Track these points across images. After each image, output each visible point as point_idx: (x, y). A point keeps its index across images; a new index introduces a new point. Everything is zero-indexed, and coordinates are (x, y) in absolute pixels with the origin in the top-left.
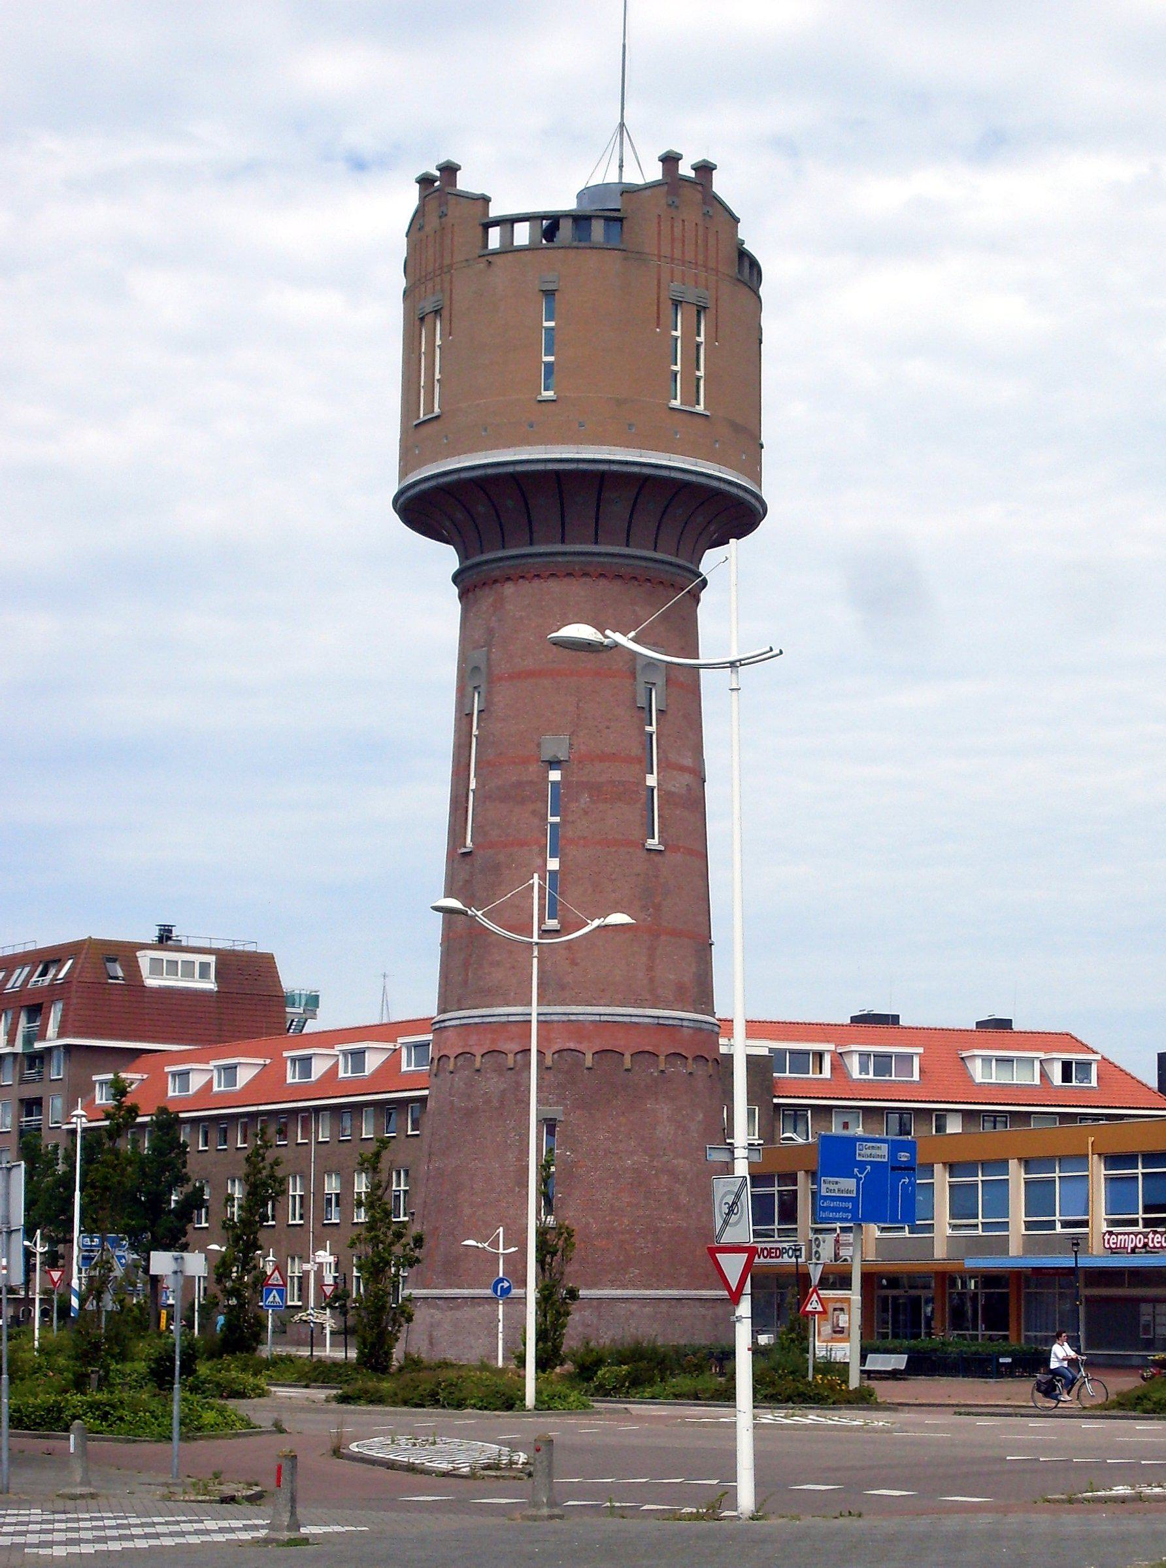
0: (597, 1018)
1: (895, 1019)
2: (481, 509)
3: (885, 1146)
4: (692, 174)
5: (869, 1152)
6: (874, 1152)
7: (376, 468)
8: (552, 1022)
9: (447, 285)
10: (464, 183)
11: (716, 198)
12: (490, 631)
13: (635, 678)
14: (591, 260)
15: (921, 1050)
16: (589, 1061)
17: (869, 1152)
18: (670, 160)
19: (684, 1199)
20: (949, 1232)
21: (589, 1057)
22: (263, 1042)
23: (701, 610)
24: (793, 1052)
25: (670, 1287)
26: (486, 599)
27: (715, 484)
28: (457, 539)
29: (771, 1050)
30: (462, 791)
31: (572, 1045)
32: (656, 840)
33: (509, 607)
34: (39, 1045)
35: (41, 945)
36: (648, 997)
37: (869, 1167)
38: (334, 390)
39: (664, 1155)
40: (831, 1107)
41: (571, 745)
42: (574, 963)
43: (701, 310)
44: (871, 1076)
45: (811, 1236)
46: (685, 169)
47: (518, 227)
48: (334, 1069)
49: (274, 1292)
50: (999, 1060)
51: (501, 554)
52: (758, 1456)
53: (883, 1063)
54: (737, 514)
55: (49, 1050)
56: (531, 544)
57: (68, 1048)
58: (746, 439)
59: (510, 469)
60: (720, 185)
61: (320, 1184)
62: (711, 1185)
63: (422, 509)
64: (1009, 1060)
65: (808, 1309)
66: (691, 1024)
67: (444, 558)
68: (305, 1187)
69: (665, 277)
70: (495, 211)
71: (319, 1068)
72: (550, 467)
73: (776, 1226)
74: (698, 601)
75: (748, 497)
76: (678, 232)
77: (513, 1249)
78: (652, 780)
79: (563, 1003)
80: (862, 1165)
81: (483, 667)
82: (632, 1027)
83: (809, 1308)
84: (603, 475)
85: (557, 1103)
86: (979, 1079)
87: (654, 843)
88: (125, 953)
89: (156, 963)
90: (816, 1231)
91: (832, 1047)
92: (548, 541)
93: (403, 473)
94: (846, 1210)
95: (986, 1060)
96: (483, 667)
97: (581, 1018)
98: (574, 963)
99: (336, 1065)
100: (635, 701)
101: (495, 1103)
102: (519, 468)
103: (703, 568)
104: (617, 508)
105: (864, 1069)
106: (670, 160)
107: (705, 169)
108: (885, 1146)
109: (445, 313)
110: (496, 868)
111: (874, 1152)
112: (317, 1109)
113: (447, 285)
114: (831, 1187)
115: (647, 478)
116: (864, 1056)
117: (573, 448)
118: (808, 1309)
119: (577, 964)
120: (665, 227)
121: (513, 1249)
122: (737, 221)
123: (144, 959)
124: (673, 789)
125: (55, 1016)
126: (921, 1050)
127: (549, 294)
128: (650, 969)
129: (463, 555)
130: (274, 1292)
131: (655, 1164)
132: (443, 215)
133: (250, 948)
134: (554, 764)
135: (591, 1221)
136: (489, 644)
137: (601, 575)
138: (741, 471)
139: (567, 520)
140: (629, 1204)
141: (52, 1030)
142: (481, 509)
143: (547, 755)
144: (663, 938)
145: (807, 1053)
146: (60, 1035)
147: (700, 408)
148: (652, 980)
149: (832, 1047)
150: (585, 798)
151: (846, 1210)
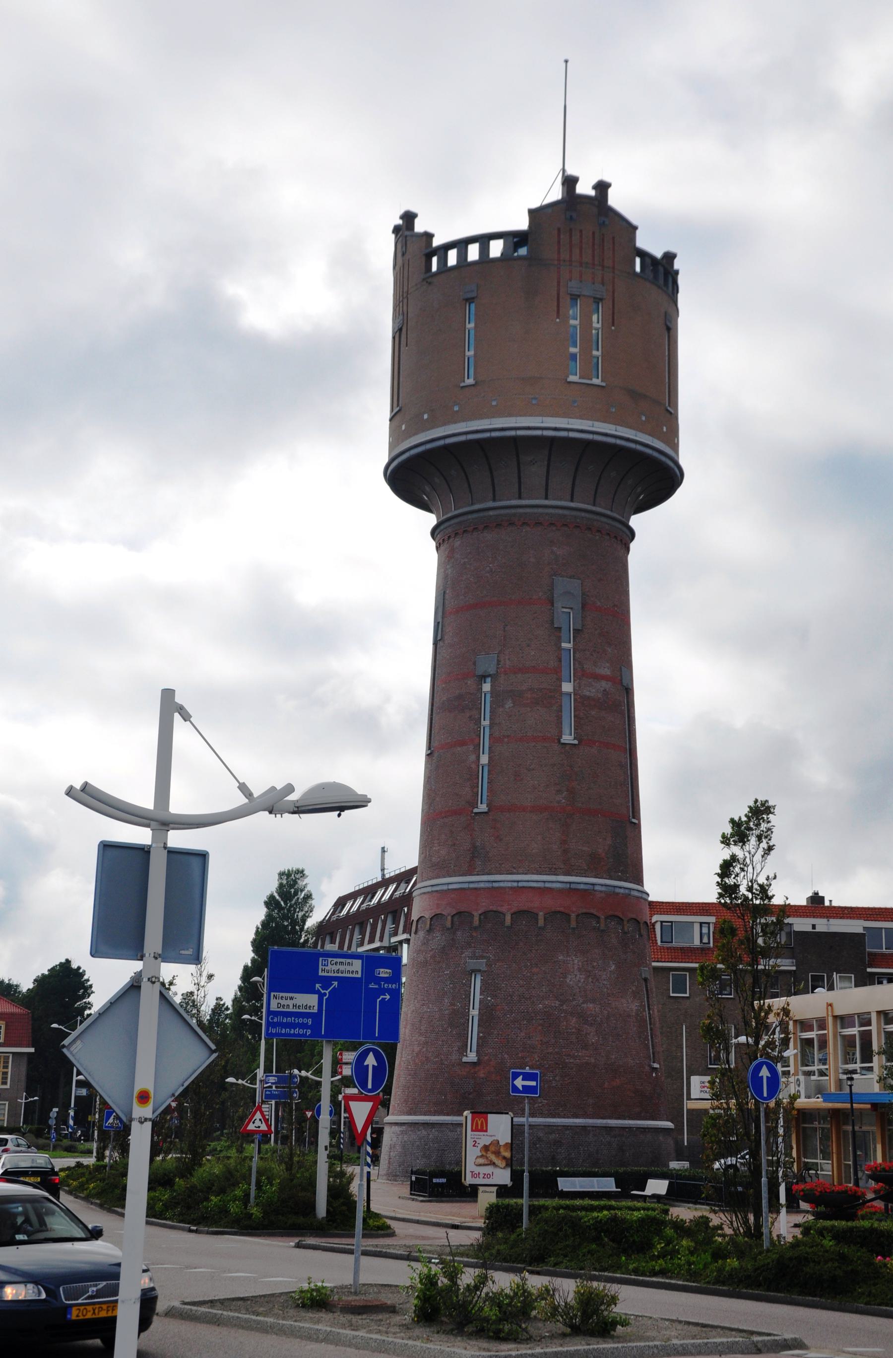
0: (515, 884)
5: (335, 968)
6: (342, 968)
8: (480, 889)
10: (420, 227)
11: (611, 210)
13: (552, 605)
17: (335, 968)
18: (570, 182)
19: (593, 1039)
23: (631, 558)
25: (576, 1116)
36: (562, 866)
37: (336, 983)
39: (574, 999)
41: (499, 661)
56: (472, 504)
60: (614, 200)
65: (249, 1128)
66: (603, 889)
70: (436, 242)
80: (326, 981)
82: (543, 891)
83: (251, 1127)
87: (568, 738)
94: (304, 1026)
97: (502, 884)
100: (552, 623)
104: (535, 472)
106: (570, 182)
107: (602, 187)
111: (342, 968)
114: (283, 1002)
115: (553, 439)
118: (249, 1128)
119: (501, 840)
122: (635, 228)
124: (588, 693)
128: (564, 842)
131: (565, 1007)
135: (506, 1056)
139: (496, 481)
143: (480, 672)
148: (565, 851)
150: (509, 704)
151: (304, 1026)
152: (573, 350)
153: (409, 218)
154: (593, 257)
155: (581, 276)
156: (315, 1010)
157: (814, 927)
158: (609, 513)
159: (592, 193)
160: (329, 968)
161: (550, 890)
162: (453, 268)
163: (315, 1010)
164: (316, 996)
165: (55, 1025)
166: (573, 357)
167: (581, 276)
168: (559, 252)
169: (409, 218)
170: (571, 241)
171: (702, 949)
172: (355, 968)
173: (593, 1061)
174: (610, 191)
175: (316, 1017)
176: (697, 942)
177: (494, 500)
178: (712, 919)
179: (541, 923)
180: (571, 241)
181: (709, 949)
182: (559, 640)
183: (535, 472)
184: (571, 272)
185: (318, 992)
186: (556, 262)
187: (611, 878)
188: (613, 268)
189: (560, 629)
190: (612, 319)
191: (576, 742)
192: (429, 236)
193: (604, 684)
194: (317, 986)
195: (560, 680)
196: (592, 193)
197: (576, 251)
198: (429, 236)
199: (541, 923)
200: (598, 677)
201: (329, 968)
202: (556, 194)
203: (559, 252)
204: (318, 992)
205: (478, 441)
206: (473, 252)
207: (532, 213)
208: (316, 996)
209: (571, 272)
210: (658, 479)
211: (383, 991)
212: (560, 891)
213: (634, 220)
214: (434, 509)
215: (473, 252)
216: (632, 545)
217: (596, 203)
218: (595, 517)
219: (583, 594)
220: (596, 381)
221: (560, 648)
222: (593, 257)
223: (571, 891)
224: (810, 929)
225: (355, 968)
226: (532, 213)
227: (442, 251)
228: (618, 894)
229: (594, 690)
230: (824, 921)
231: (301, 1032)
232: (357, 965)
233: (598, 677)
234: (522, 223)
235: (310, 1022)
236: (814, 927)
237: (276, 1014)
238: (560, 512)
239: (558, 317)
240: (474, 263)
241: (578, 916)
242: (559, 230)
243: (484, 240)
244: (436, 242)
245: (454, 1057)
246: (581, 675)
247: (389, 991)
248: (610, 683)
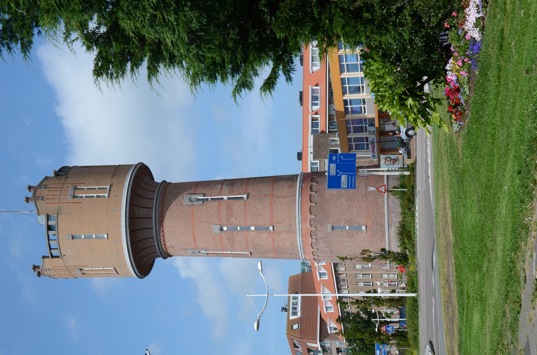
1: (301, 93)
2: (143, 253)
3: (331, 165)
4: (32, 192)
9: (72, 268)
12: (181, 249)
14: (61, 226)
15: (310, 86)
16: (313, 216)
20: (365, 94)
21: (312, 216)
22: (316, 285)
23: (173, 181)
24: (312, 127)
26: (170, 251)
27: (131, 182)
28: (153, 259)
29: (312, 134)
30: (232, 255)
31: (309, 222)
32: (244, 196)
33: (173, 244)
34: (320, 349)
35: (289, 348)
40: (329, 114)
42: (283, 222)
43: (76, 189)
44: (319, 102)
45: (367, 133)
46: (30, 195)
48: (323, 266)
50: (313, 61)
51: (157, 247)
52: (405, 297)
53: (315, 98)
55: (321, 346)
56: (153, 238)
57: (320, 341)
59: (130, 247)
61: (359, 270)
64: (313, 57)
68: (359, 274)
69: (65, 201)
71: (323, 271)
72: (128, 235)
73: (365, 143)
75: (136, 169)
76: (51, 197)
78: (225, 198)
79: (296, 225)
81: (193, 251)
84: (130, 218)
85: (327, 226)
86: (319, 68)
88: (291, 324)
89: (295, 314)
90: (366, 131)
91: (310, 115)
92: (152, 233)
94: (352, 179)
95: (313, 65)
96: (193, 251)
98: (283, 222)
99: (322, 266)
101: (328, 244)
102: (129, 244)
103: (160, 182)
104: (141, 212)
105: (317, 104)
108: (331, 165)
109: (81, 268)
110: (255, 246)
112: (335, 271)
113: (72, 268)
116: (313, 104)
117: (123, 238)
120: (49, 201)
122: (46, 177)
123: (292, 318)
125: (310, 345)
126: (310, 86)
127: (73, 237)
128: (284, 197)
129: (158, 256)
132: (50, 270)
133: (288, 283)
134: (221, 229)
136: (186, 249)
138: (127, 172)
140: (358, 202)
141: (315, 345)
142: (143, 253)
144: (274, 193)
145: (312, 123)
146: (316, 343)
147: (108, 187)
148: (287, 197)
149: (310, 115)
150: (232, 219)
151: (352, 179)
157: (311, 153)
158: (156, 193)
160: (333, 172)
172: (333, 166)
175: (348, 175)
177: (152, 228)
183: (141, 212)
197: (55, 197)
201: (333, 172)
205: (130, 232)
210: (142, 172)
211: (340, 158)
214: (153, 259)
216: (168, 181)
218: (160, 191)
224: (312, 155)
225: (333, 166)
230: (309, 149)
232: (332, 165)
236: (311, 153)
238: (158, 203)
245: (364, 235)
247: (340, 157)
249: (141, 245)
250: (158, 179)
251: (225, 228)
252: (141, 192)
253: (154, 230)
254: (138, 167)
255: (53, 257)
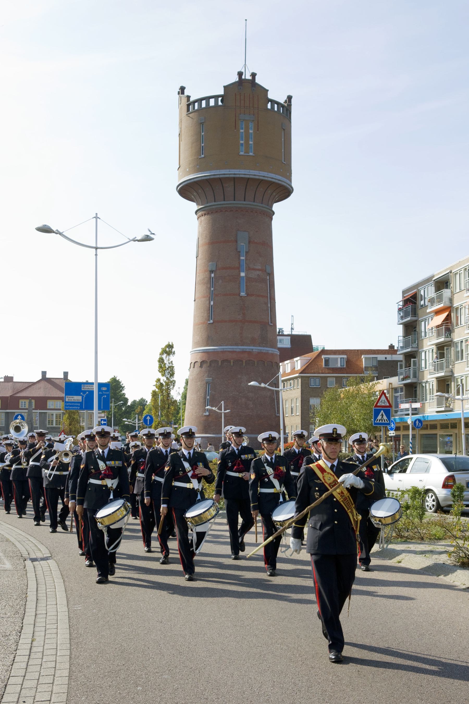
2: (200, 191)
5: (87, 387)
6: (89, 387)
7: (176, 178)
17: (87, 387)
37: (87, 393)
38: (166, 155)
41: (217, 265)
47: (211, 100)
49: (382, 411)
54: (285, 192)
58: (285, 167)
60: (258, 80)
62: (47, 402)
63: (186, 191)
66: (257, 351)
67: (193, 206)
70: (192, 99)
74: (272, 219)
77: (228, 411)
80: (84, 392)
82: (233, 352)
84: (220, 179)
87: (243, 294)
93: (179, 181)
94: (78, 406)
103: (274, 209)
106: (240, 74)
111: (89, 387)
121: (228, 411)
130: (382, 411)
137: (226, 211)
142: (200, 191)
150: (220, 281)
151: (78, 406)
152: (242, 142)
153: (182, 89)
154: (250, 104)
155: (244, 112)
156: (81, 401)
157: (386, 358)
159: (250, 78)
161: (235, 352)
162: (204, 108)
163: (81, 401)
164: (81, 397)
165: (252, 383)
166: (242, 144)
167: (244, 112)
168: (236, 103)
169: (182, 89)
170: (240, 98)
171: (341, 368)
173: (251, 414)
174: (256, 77)
175: (81, 403)
176: (339, 366)
177: (215, 202)
178: (345, 356)
179: (232, 364)
180: (240, 98)
181: (344, 368)
182: (239, 256)
184: (240, 110)
185: (81, 395)
186: (234, 107)
187: (260, 346)
188: (258, 108)
189: (240, 252)
190: (257, 128)
191: (246, 295)
192: (188, 97)
193: (258, 272)
194: (81, 393)
195: (240, 272)
196: (250, 78)
197: (242, 102)
198: (188, 97)
199: (232, 364)
200: (254, 269)
202: (235, 78)
203: (236, 103)
204: (81, 395)
206: (204, 104)
207: (225, 87)
208: (81, 397)
209: (240, 110)
212: (239, 352)
213: (267, 88)
215: (204, 104)
216: (274, 217)
217: (251, 82)
219: (249, 237)
220: (251, 154)
221: (239, 259)
222: (250, 104)
223: (243, 352)
226: (225, 87)
227: (200, 101)
228: (263, 352)
229: (254, 274)
231: (76, 408)
233: (254, 269)
234: (222, 92)
235: (79, 405)
236: (386, 358)
237: (68, 402)
239: (235, 129)
240: (212, 107)
241: (246, 361)
242: (236, 94)
243: (207, 99)
244: (192, 99)
246: (249, 269)
247: (106, 394)
248: (260, 272)
249: (262, 189)
250: (276, 207)
251: (213, 275)
252: (262, 189)
253: (214, 203)
254: (289, 187)
255: (188, 106)
